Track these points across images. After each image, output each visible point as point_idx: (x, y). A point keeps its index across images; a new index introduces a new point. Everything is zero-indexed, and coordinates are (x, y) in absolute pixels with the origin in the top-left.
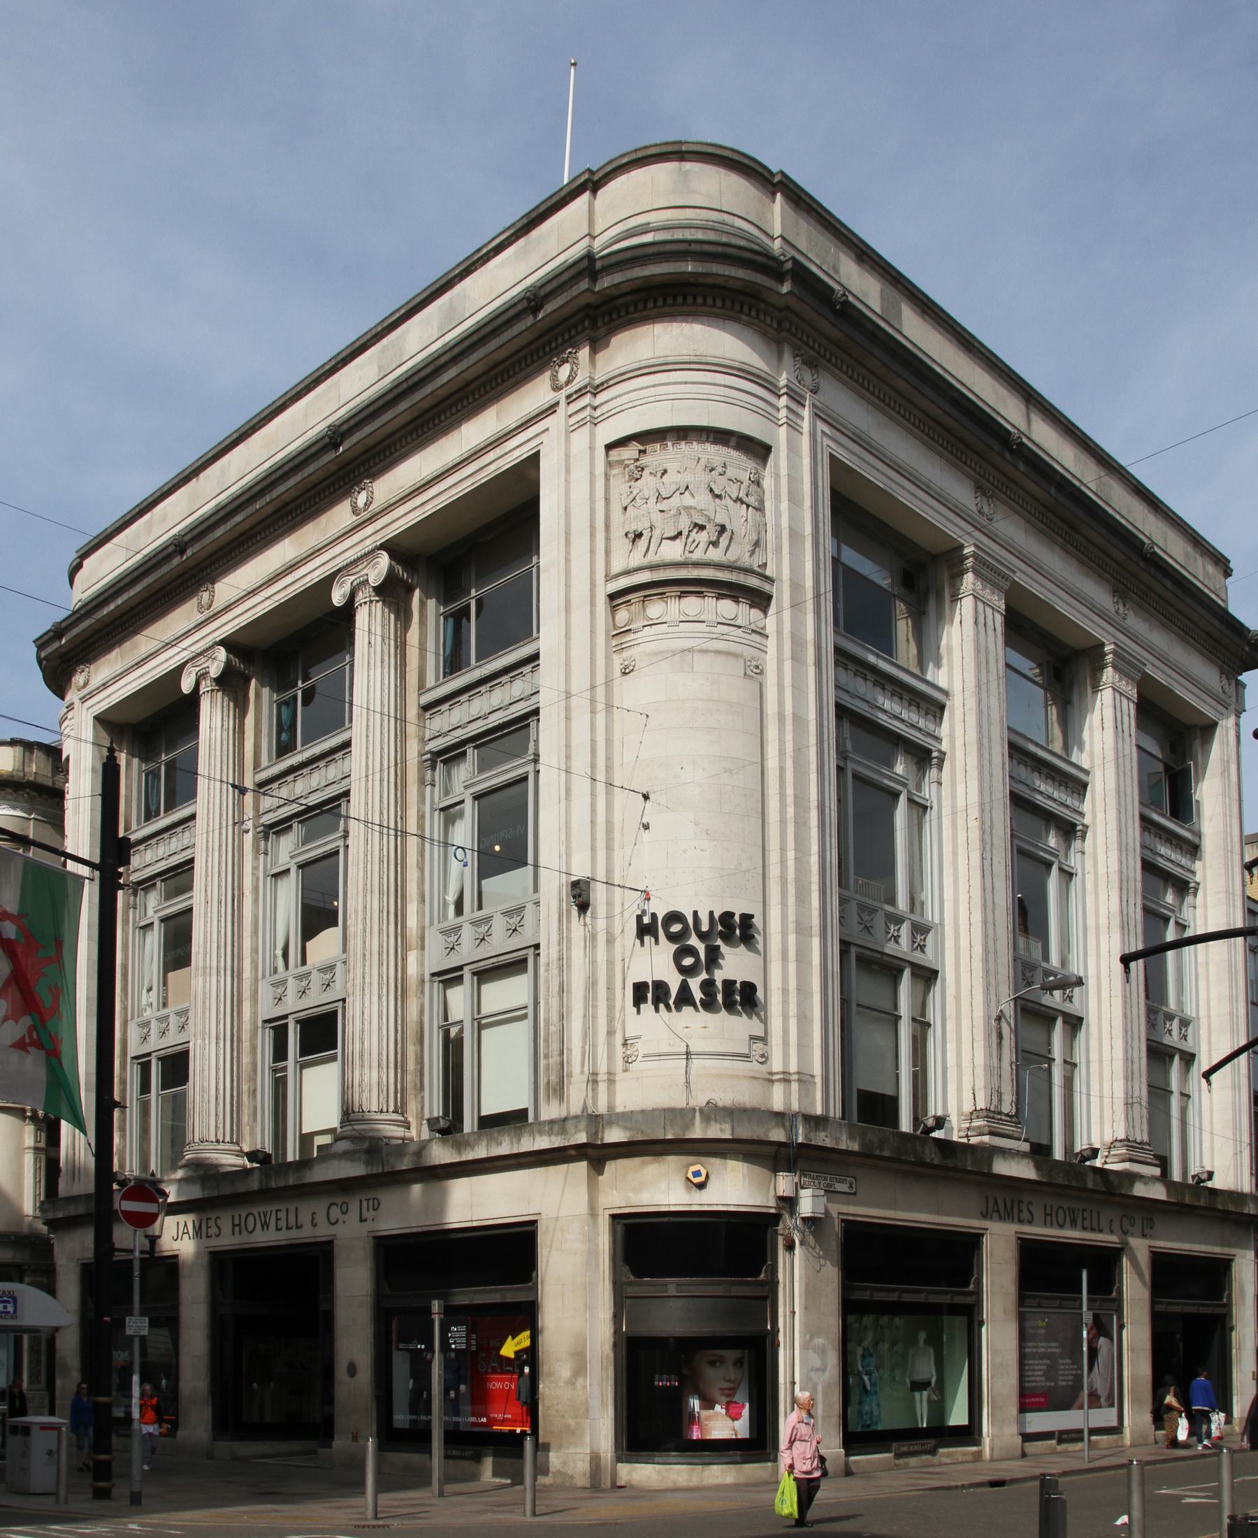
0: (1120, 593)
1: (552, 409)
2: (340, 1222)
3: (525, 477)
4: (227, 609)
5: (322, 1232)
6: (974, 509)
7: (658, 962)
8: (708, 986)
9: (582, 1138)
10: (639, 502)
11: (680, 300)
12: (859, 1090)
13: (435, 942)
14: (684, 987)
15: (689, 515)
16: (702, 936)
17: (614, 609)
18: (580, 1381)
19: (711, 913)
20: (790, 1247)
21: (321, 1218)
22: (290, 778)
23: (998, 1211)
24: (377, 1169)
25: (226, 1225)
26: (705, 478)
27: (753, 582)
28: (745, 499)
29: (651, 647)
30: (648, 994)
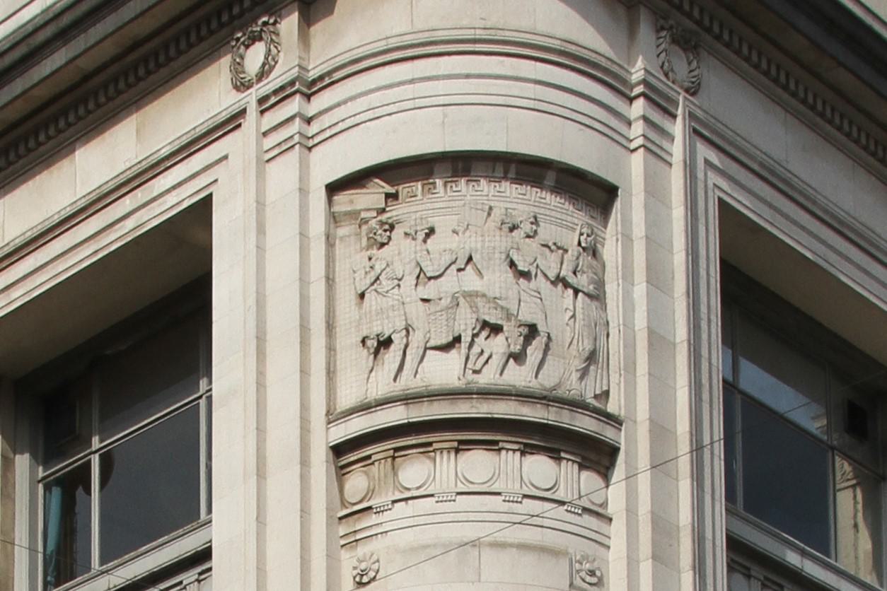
1: (233, 122)
3: (192, 227)
10: (385, 284)
15: (474, 308)
17: (342, 471)
26: (501, 242)
28: (571, 279)
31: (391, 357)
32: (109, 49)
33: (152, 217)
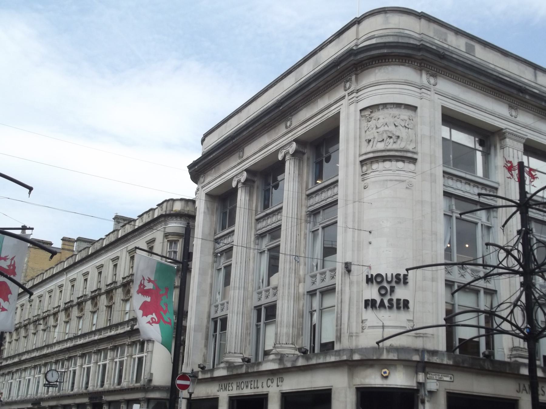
1: (343, 98)
3: (336, 117)
4: (247, 159)
6: (508, 115)
7: (372, 293)
8: (390, 301)
9: (345, 358)
10: (370, 129)
11: (384, 61)
12: (461, 340)
13: (309, 280)
14: (382, 301)
15: (387, 133)
16: (389, 282)
17: (361, 113)
19: (392, 274)
20: (423, 402)
21: (265, 384)
22: (266, 218)
23: (526, 390)
24: (282, 367)
25: (235, 387)
26: (392, 120)
27: (409, 155)
28: (407, 126)
29: (373, 179)
30: (370, 304)
31: (371, 143)
33: (330, 115)
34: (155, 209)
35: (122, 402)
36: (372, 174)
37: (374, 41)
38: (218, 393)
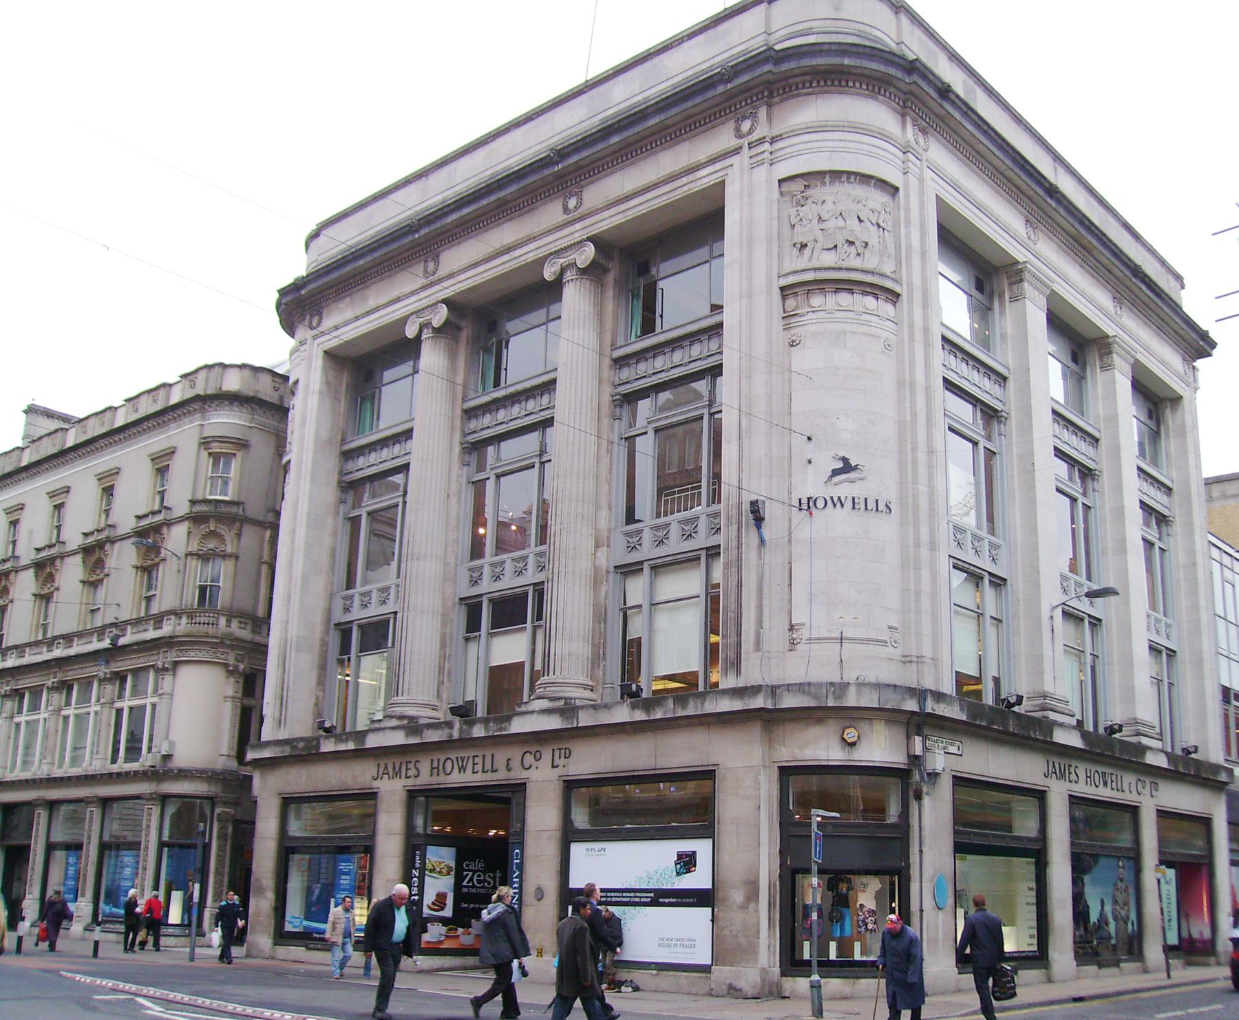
0: (1118, 299)
1: (737, 151)
2: (534, 768)
5: (518, 774)
10: (805, 222)
11: (836, 83)
17: (784, 298)
18: (752, 905)
25: (425, 767)
27: (888, 284)
31: (807, 251)
32: (679, 118)
34: (171, 385)
35: (37, 805)
36: (811, 316)
37: (811, 39)
38: (376, 784)
